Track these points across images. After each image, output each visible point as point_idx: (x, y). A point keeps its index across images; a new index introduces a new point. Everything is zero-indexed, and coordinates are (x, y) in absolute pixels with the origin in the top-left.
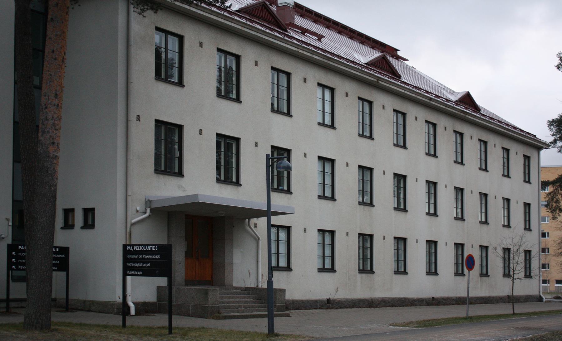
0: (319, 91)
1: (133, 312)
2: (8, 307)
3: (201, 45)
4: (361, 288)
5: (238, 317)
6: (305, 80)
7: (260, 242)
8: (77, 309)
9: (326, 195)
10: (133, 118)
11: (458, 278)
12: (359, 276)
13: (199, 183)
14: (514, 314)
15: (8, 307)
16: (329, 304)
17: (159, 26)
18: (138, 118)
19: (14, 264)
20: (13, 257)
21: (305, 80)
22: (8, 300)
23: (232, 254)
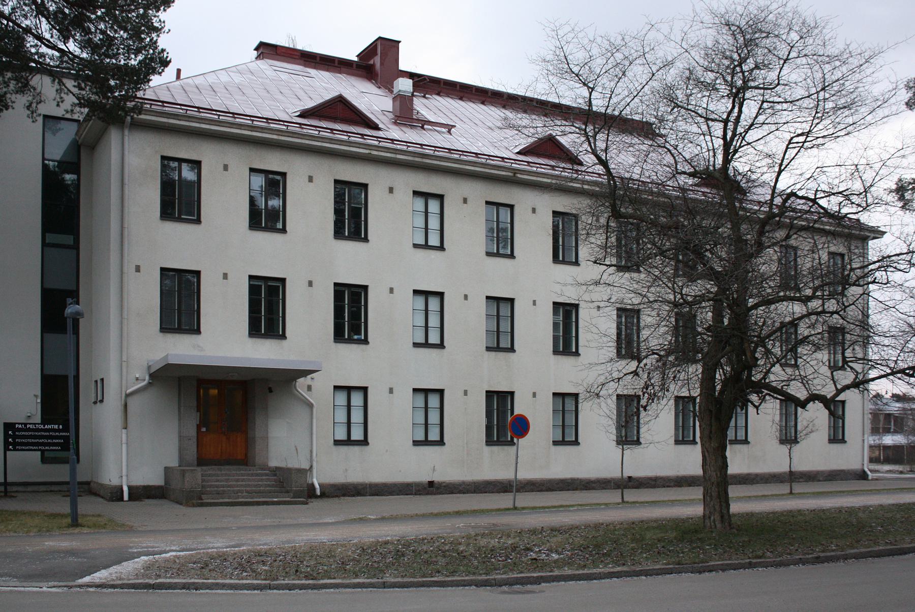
0: (419, 204)
1: (126, 497)
2: (6, 491)
3: (226, 168)
4: (494, 464)
5: (221, 504)
6: (391, 190)
7: (315, 410)
8: (96, 494)
9: (431, 341)
10: (129, 269)
11: (682, 448)
12: (487, 450)
13: (224, 340)
14: (515, 508)
15: (6, 491)
16: (431, 488)
17: (338, 178)
18: (138, 269)
19: (11, 444)
20: (10, 436)
21: (391, 190)
22: (6, 484)
23: (267, 426)
